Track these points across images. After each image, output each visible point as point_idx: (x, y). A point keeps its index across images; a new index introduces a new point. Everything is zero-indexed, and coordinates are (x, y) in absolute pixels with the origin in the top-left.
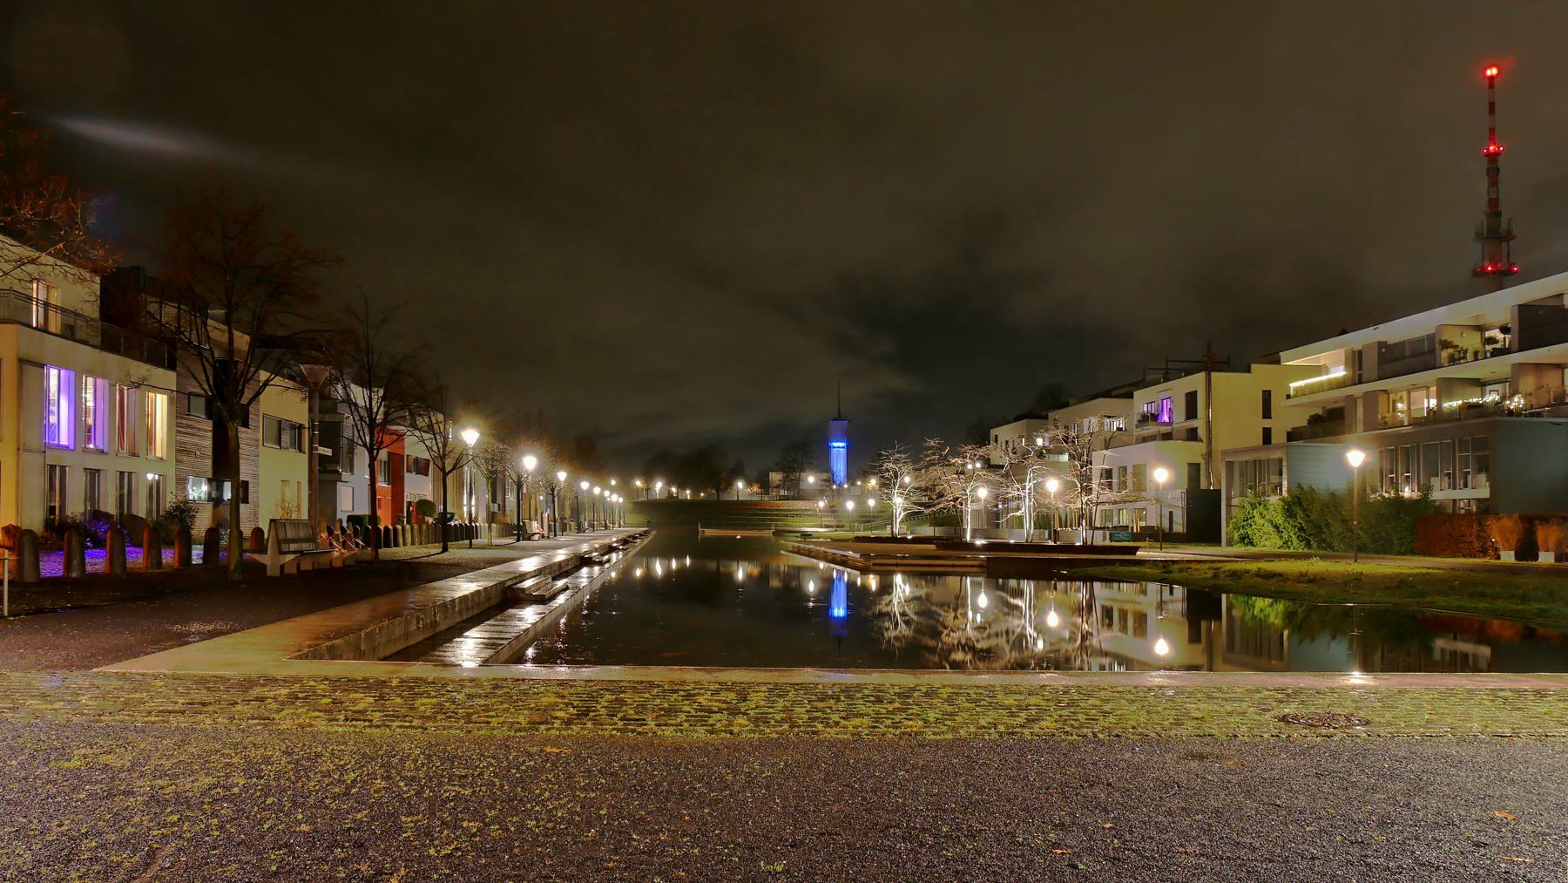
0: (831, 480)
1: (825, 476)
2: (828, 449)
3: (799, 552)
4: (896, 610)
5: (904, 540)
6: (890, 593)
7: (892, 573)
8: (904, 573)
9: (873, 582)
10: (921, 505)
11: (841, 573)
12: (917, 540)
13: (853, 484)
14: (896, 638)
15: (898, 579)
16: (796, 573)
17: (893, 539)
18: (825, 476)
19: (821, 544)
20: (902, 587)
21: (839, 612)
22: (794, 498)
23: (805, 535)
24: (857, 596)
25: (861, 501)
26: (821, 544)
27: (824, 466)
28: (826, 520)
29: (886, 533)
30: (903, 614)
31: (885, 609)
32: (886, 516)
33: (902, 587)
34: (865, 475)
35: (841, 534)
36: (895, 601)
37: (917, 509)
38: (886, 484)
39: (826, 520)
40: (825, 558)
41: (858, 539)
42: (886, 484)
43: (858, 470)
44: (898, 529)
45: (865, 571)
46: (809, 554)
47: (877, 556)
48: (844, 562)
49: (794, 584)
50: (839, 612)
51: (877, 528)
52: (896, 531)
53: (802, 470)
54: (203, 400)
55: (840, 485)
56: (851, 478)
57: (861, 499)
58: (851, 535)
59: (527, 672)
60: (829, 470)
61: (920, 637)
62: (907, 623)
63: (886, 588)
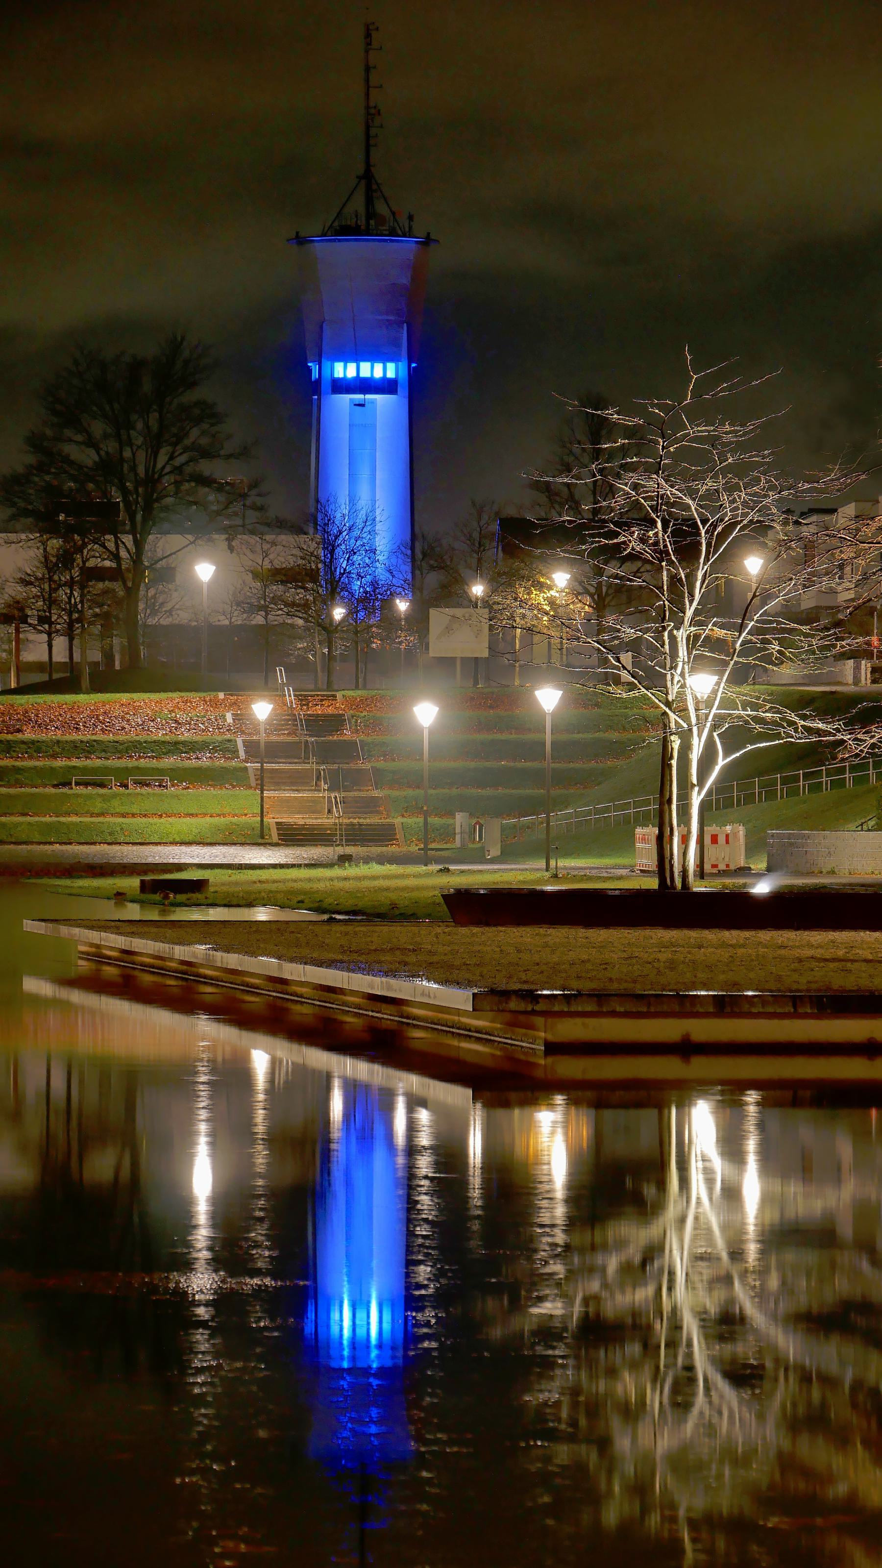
0: (316, 577)
1: (286, 551)
2: (308, 395)
3: (128, 982)
4: (687, 1299)
5: (732, 910)
6: (647, 1208)
7: (656, 1098)
8: (730, 1094)
9: (552, 1140)
10: (832, 705)
11: (368, 1107)
12: (798, 909)
13: (450, 593)
14: (683, 1464)
15: (702, 1123)
16: (119, 1112)
17: (668, 905)
18: (286, 551)
19: (250, 937)
20: (721, 1173)
21: (360, 1316)
22: (105, 680)
23: (169, 888)
24: (474, 1237)
25: (490, 683)
26: (250, 937)
27: (282, 496)
28: (288, 805)
29: (628, 868)
30: (726, 1324)
31: (622, 1301)
32: (626, 762)
33: (721, 1173)
34: (518, 541)
35: (372, 875)
36: (678, 1257)
37: (802, 728)
38: (628, 595)
39: (288, 805)
40: (273, 1017)
41: (473, 907)
42: (628, 595)
43: (466, 533)
44: (700, 848)
45: (507, 1085)
46: (183, 993)
47: (570, 1003)
48: (385, 1041)
49: (101, 1166)
50: (360, 1316)
51: (580, 841)
52: (687, 855)
53: (411, 601)
54: (45, 658)
55: (373, 601)
56: (431, 561)
57: (490, 683)
58: (427, 880)
59: (425, 993)
60: (311, 516)
61: (816, 1452)
62: (742, 1376)
63: (624, 1184)
